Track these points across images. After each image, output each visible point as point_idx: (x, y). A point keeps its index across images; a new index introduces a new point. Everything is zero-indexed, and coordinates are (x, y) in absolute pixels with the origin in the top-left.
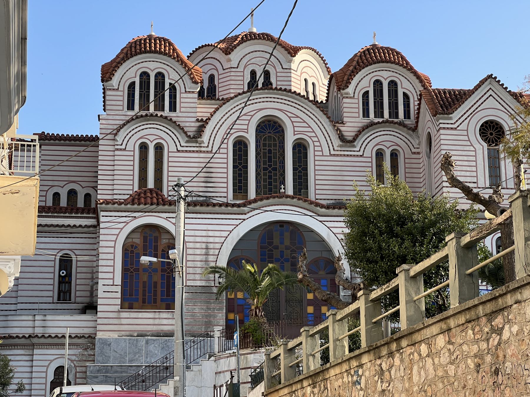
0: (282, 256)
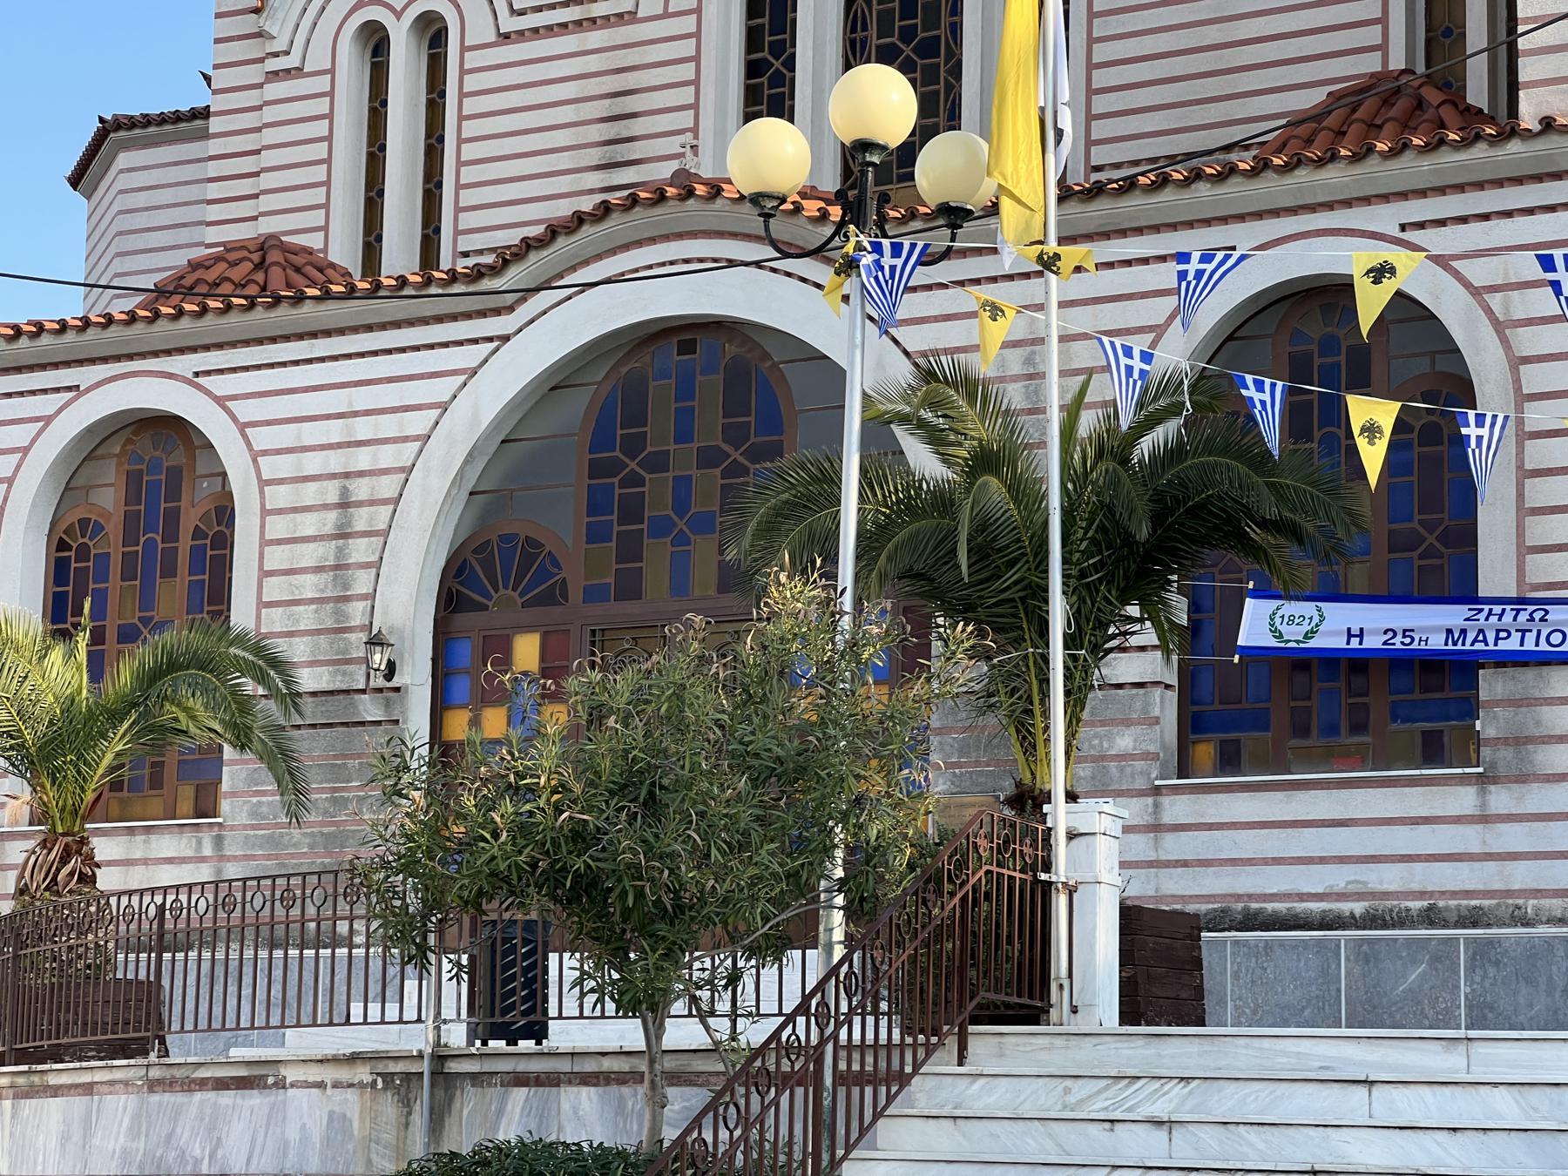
0: (681, 506)
